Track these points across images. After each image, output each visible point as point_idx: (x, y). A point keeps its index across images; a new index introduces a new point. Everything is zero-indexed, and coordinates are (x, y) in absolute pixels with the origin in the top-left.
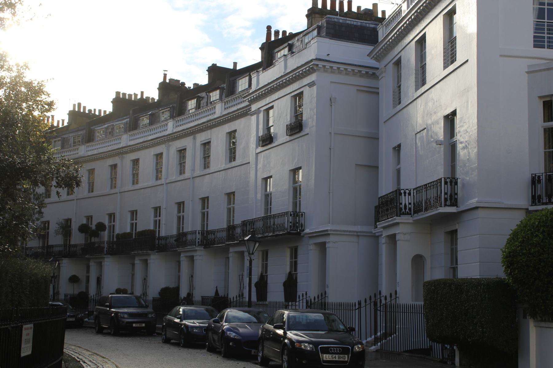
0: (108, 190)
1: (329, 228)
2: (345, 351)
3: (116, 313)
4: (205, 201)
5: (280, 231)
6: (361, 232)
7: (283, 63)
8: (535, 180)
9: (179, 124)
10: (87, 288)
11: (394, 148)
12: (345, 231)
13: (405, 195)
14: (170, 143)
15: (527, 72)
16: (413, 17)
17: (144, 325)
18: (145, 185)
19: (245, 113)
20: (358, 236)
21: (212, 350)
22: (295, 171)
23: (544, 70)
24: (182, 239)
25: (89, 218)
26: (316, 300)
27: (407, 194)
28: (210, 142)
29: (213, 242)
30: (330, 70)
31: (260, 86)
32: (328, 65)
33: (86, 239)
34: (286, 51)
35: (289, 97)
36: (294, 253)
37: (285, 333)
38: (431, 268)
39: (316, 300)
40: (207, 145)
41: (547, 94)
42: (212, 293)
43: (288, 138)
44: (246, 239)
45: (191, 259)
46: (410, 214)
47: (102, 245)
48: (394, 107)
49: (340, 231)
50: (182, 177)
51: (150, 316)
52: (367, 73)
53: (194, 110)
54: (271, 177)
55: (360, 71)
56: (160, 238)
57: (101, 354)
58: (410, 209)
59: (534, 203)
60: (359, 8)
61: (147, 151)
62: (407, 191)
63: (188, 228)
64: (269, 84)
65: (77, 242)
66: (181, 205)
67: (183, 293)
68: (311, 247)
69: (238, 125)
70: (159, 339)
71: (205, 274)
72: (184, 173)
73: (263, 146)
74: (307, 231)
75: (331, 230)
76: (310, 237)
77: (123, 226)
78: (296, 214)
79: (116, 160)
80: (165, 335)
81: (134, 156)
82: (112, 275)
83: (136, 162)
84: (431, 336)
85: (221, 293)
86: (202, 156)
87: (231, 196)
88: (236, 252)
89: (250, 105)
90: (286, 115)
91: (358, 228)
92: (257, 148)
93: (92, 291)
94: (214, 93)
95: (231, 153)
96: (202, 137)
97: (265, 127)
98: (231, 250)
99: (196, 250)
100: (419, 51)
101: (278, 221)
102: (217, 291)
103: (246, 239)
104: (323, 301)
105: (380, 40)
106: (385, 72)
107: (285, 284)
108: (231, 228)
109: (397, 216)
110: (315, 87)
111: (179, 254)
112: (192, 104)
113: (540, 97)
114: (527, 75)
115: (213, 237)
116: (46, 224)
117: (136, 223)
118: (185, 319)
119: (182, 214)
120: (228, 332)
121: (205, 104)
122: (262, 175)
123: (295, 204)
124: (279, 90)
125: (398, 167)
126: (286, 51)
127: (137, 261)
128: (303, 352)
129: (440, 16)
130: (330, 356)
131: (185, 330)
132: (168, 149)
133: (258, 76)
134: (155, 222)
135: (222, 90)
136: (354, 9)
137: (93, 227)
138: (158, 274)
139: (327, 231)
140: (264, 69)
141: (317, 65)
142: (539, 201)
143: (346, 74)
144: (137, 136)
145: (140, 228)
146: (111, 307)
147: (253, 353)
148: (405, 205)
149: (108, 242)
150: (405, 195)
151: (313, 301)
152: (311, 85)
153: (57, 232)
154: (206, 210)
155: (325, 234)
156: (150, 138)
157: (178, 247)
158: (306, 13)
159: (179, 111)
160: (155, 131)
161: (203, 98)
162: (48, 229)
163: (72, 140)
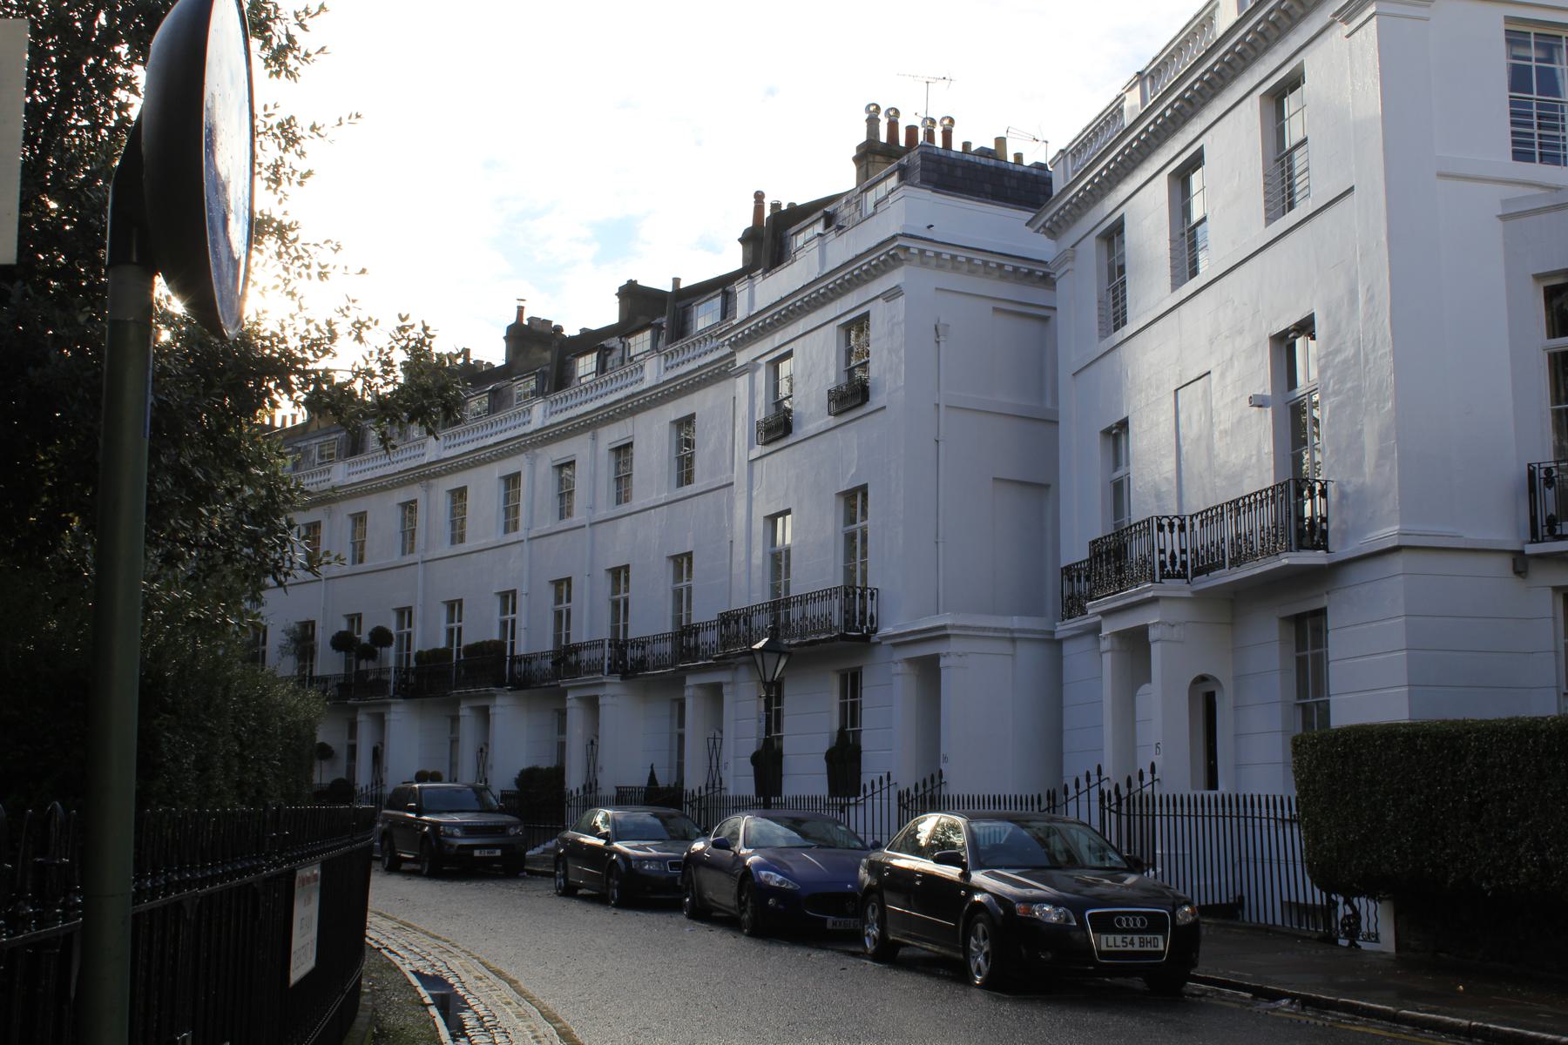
0: (396, 558)
1: (949, 622)
2: (1155, 924)
3: (435, 826)
4: (619, 575)
5: (820, 632)
6: (1020, 631)
7: (816, 253)
8: (1535, 480)
9: (559, 407)
10: (351, 770)
11: (1107, 432)
12: (984, 629)
13: (1172, 531)
14: (538, 451)
15: (1503, 217)
16: (1168, 113)
17: (498, 853)
18: (482, 543)
19: (721, 373)
20: (1013, 640)
21: (703, 913)
22: (772, 519)
23: (1547, 209)
24: (566, 659)
25: (356, 619)
26: (921, 791)
27: (1176, 529)
28: (630, 445)
29: (641, 664)
30: (934, 262)
31: (759, 307)
32: (931, 250)
33: (348, 665)
34: (819, 228)
35: (833, 327)
36: (852, 684)
37: (965, 875)
38: (1236, 708)
39: (921, 791)
40: (623, 451)
41: (1556, 268)
42: (641, 780)
43: (832, 421)
44: (757, 646)
45: (593, 704)
46: (1186, 577)
47: (384, 677)
48: (1102, 337)
49: (974, 628)
50: (565, 524)
51: (512, 831)
52: (1016, 269)
53: (590, 378)
54: (1306, 327)
55: (1000, 266)
56: (515, 659)
57: (422, 926)
58: (1184, 564)
59: (1535, 537)
60: (966, 145)
61: (484, 469)
62: (1176, 522)
63: (579, 635)
64: (782, 300)
65: (328, 672)
66: (562, 587)
67: (574, 780)
68: (900, 668)
69: (698, 403)
70: (546, 887)
71: (625, 736)
72: (570, 514)
73: (765, 444)
74: (885, 630)
75: (954, 627)
76: (895, 645)
77: (429, 634)
78: (855, 593)
79: (415, 492)
80: (565, 876)
81: (454, 481)
82: (407, 743)
83: (459, 494)
84: (1324, 876)
85: (663, 780)
86: (612, 476)
87: (682, 563)
88: (700, 686)
89: (732, 354)
90: (826, 369)
91: (1015, 622)
92: (751, 447)
93: (363, 779)
94: (639, 337)
95: (680, 466)
96: (612, 435)
97: (771, 400)
98: (690, 681)
99: (603, 684)
100: (1179, 197)
101: (813, 610)
102: (652, 775)
103: (757, 646)
104: (936, 791)
105: (1055, 192)
106: (1073, 259)
107: (830, 756)
108: (685, 632)
109: (1153, 581)
110: (901, 300)
111: (562, 694)
112: (586, 365)
113: (1538, 277)
114: (1499, 223)
115: (638, 653)
116: (260, 632)
117: (460, 629)
118: (617, 840)
119: (565, 605)
120: (763, 873)
121: (617, 362)
122: (762, 509)
123: (849, 572)
124: (808, 312)
125: (1117, 475)
126: (819, 228)
127: (465, 711)
128: (1034, 927)
129: (1248, 100)
130: (1119, 938)
131: (622, 866)
132: (533, 465)
133: (752, 287)
134: (504, 624)
135: (657, 330)
136: (957, 146)
137: (364, 638)
138: (513, 739)
139: (944, 627)
140: (766, 271)
141: (907, 249)
142: (1552, 532)
143: (971, 272)
144: (462, 439)
145: (469, 639)
146: (419, 811)
147: (829, 925)
148: (1173, 555)
149: (398, 670)
150: (1172, 531)
151: (912, 792)
152: (891, 295)
153: (283, 650)
154: (859, 524)
155: (939, 635)
156: (491, 441)
157: (558, 677)
158: (854, 153)
159: (558, 379)
160: (504, 426)
161: (611, 350)
162: (264, 643)
163: (316, 451)
